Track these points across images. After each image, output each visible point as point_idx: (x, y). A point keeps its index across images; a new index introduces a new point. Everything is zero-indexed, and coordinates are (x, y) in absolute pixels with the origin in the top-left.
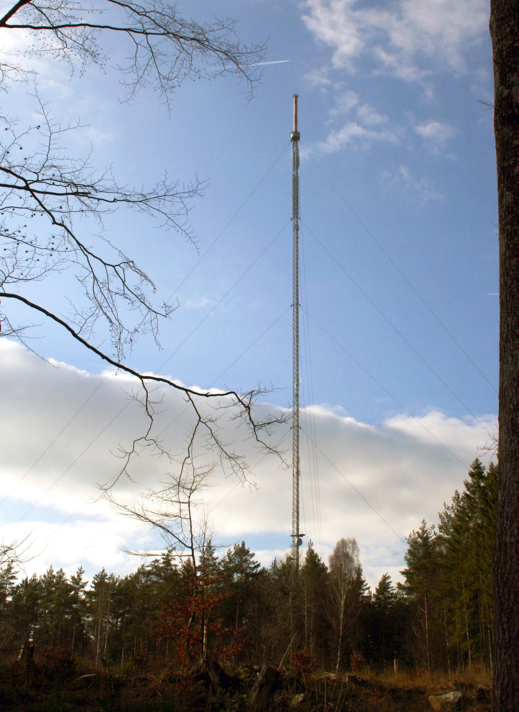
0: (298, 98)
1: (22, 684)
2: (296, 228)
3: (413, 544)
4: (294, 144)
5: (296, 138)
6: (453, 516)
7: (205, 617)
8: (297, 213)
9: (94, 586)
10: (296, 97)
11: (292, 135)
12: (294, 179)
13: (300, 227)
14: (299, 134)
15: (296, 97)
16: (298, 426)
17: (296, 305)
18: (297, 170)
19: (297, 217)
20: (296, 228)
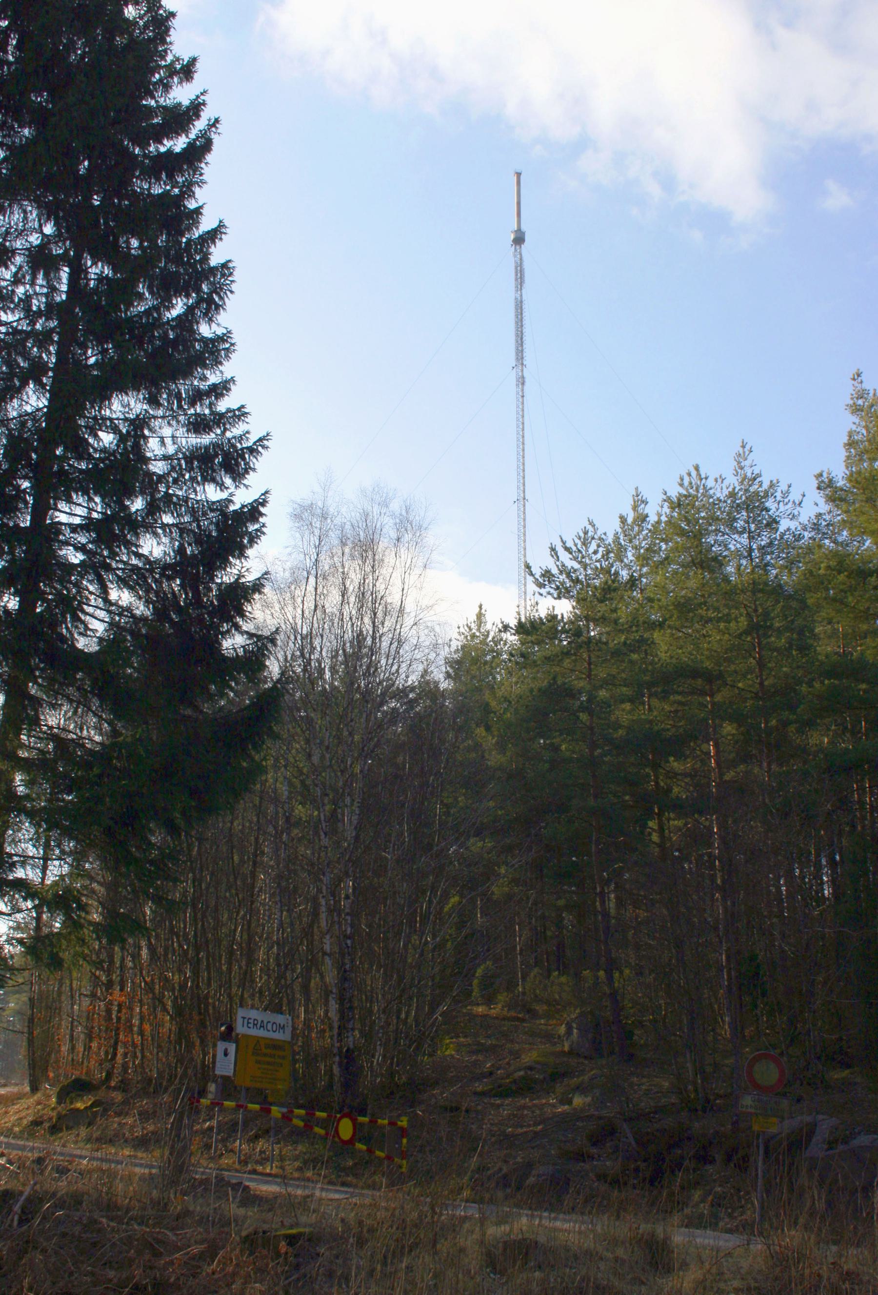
0: (522, 177)
1: (58, 1029)
2: (522, 381)
3: (192, 78)
4: (516, 250)
5: (519, 240)
6: (606, 1216)
7: (396, 1284)
8: (522, 358)
9: (48, 882)
10: (519, 175)
11: (512, 237)
12: (516, 305)
13: (527, 380)
14: (524, 233)
15: (519, 175)
16: (524, 499)
17: (523, 499)
18: (521, 289)
19: (522, 364)
20: (522, 381)
